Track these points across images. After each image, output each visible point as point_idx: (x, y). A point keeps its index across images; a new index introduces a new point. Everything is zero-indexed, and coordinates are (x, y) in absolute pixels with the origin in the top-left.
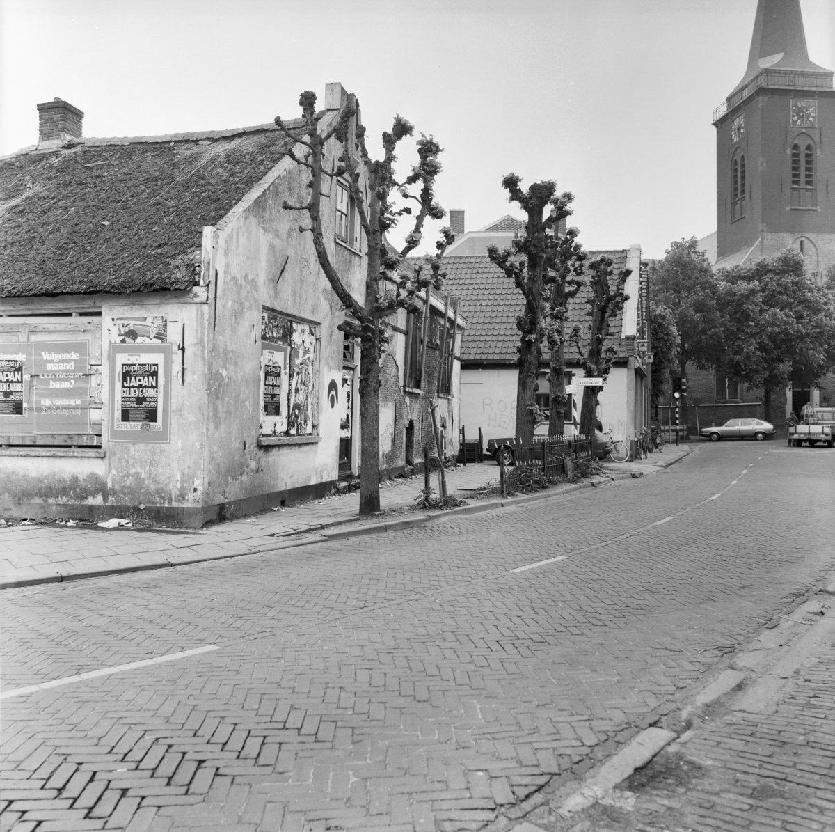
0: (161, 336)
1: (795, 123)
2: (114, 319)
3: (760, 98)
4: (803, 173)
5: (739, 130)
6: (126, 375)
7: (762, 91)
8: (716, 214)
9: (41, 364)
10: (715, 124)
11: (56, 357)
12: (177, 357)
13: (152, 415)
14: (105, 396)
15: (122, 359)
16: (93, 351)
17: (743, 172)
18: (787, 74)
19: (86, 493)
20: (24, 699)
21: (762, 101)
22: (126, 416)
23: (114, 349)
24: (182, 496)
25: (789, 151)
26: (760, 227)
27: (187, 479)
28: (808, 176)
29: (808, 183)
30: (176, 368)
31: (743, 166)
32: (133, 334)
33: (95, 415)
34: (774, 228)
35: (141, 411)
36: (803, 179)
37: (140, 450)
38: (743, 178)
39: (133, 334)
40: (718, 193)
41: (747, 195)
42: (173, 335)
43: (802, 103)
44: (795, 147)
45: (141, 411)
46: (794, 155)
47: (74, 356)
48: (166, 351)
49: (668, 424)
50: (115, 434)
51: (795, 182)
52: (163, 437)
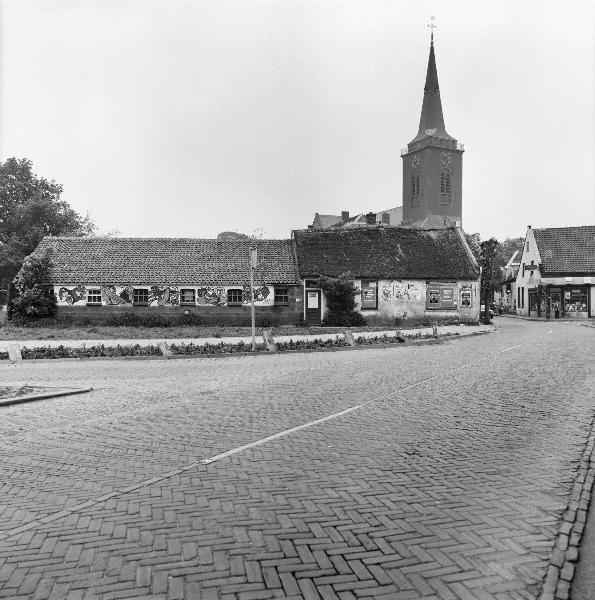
0: (471, 288)
1: (443, 163)
2: (460, 285)
3: (429, 150)
4: (446, 187)
5: (416, 163)
6: (463, 296)
7: (429, 147)
8: (402, 199)
9: (443, 293)
10: (403, 157)
11: (446, 291)
12: (474, 292)
13: (469, 304)
14: (459, 300)
15: (462, 292)
16: (455, 291)
17: (418, 184)
18: (439, 140)
19: (454, 319)
20: (9, 519)
21: (429, 152)
22: (463, 304)
23: (461, 290)
24: (475, 320)
25: (440, 177)
26: (428, 212)
27: (476, 316)
28: (448, 189)
29: (448, 192)
30: (474, 294)
31: (418, 181)
32: (465, 287)
33: (455, 303)
34: (435, 213)
35: (466, 303)
36: (446, 190)
37: (466, 311)
38: (418, 187)
39: (465, 287)
40: (404, 191)
41: (421, 195)
42: (473, 288)
43: (446, 154)
44: (443, 175)
45: (466, 303)
46: (442, 179)
47: (451, 291)
48: (472, 291)
49: (285, 297)
50: (461, 307)
51: (443, 192)
52: (471, 308)
